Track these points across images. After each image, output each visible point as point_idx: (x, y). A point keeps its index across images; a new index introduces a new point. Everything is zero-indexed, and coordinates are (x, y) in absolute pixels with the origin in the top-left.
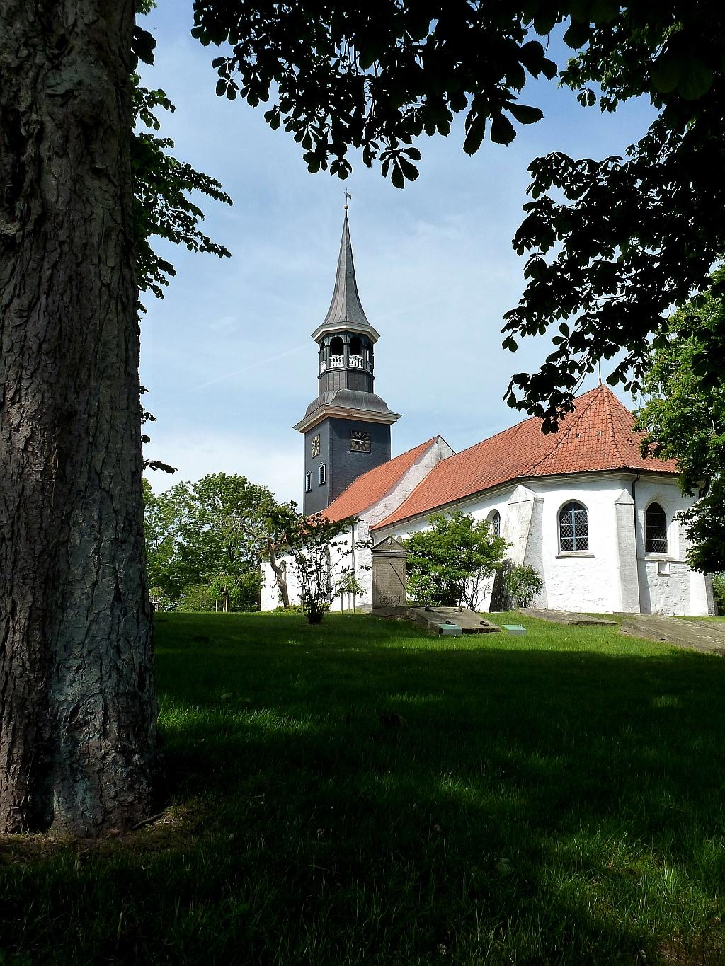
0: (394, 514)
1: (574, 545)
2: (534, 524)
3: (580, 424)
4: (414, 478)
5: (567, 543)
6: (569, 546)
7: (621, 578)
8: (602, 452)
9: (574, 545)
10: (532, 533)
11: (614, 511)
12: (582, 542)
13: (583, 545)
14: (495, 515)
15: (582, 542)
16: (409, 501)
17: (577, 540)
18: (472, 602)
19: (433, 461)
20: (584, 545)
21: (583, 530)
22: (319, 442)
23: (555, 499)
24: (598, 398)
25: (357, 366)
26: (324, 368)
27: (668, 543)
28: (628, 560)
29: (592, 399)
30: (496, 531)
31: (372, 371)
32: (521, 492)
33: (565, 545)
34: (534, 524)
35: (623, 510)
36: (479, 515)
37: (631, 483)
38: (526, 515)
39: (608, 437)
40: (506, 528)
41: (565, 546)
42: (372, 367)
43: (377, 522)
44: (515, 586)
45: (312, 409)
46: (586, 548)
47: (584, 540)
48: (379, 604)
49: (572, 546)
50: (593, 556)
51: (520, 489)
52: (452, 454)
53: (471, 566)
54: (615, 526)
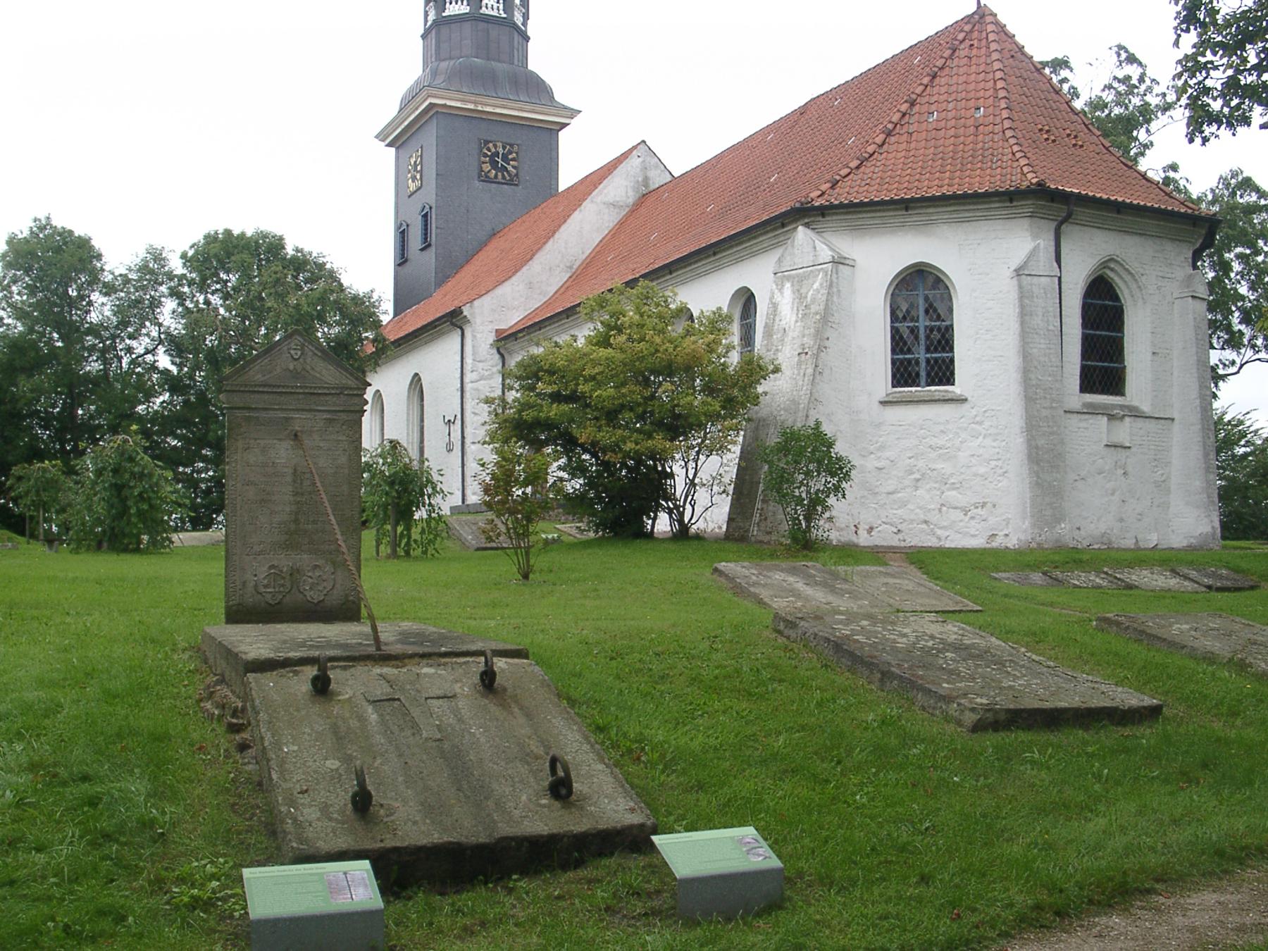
0: (547, 304)
1: (923, 374)
2: (825, 323)
3: (936, 90)
4: (583, 231)
5: (906, 369)
6: (910, 375)
7: (1030, 456)
8: (986, 153)
9: (923, 374)
10: (827, 343)
11: (1013, 295)
12: (940, 368)
13: (943, 373)
14: (746, 300)
15: (940, 368)
16: (579, 275)
17: (928, 361)
18: (682, 514)
19: (631, 193)
20: (944, 374)
21: (943, 340)
22: (421, 163)
23: (880, 257)
24: (975, 34)
25: (495, 13)
26: (431, 17)
27: (1128, 370)
28: (1045, 413)
29: (961, 36)
30: (747, 338)
31: (525, 24)
32: (806, 244)
33: (903, 374)
34: (825, 323)
35: (1035, 290)
36: (706, 295)
37: (1054, 225)
38: (813, 300)
39: (998, 120)
40: (769, 332)
41: (902, 375)
42: (526, 17)
43: (512, 319)
44: (793, 474)
45: (409, 100)
46: (950, 380)
47: (944, 361)
48: (250, 599)
49: (918, 375)
50: (962, 400)
51: (802, 234)
52: (669, 178)
53: (677, 426)
54: (1014, 326)
